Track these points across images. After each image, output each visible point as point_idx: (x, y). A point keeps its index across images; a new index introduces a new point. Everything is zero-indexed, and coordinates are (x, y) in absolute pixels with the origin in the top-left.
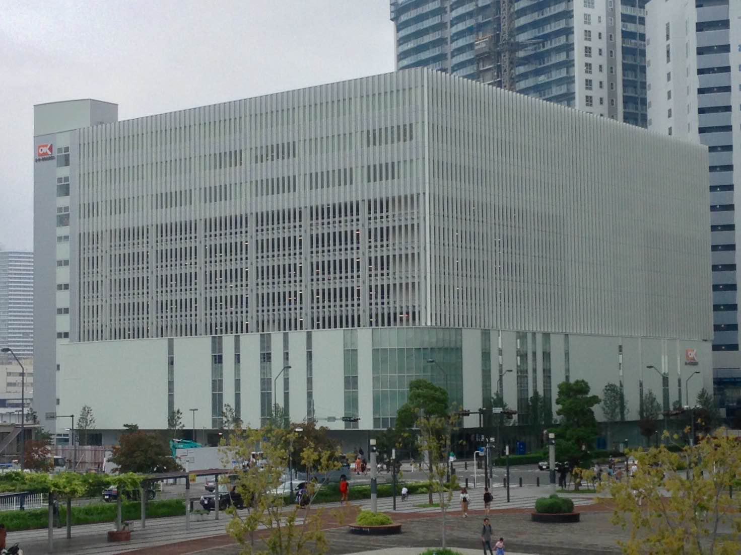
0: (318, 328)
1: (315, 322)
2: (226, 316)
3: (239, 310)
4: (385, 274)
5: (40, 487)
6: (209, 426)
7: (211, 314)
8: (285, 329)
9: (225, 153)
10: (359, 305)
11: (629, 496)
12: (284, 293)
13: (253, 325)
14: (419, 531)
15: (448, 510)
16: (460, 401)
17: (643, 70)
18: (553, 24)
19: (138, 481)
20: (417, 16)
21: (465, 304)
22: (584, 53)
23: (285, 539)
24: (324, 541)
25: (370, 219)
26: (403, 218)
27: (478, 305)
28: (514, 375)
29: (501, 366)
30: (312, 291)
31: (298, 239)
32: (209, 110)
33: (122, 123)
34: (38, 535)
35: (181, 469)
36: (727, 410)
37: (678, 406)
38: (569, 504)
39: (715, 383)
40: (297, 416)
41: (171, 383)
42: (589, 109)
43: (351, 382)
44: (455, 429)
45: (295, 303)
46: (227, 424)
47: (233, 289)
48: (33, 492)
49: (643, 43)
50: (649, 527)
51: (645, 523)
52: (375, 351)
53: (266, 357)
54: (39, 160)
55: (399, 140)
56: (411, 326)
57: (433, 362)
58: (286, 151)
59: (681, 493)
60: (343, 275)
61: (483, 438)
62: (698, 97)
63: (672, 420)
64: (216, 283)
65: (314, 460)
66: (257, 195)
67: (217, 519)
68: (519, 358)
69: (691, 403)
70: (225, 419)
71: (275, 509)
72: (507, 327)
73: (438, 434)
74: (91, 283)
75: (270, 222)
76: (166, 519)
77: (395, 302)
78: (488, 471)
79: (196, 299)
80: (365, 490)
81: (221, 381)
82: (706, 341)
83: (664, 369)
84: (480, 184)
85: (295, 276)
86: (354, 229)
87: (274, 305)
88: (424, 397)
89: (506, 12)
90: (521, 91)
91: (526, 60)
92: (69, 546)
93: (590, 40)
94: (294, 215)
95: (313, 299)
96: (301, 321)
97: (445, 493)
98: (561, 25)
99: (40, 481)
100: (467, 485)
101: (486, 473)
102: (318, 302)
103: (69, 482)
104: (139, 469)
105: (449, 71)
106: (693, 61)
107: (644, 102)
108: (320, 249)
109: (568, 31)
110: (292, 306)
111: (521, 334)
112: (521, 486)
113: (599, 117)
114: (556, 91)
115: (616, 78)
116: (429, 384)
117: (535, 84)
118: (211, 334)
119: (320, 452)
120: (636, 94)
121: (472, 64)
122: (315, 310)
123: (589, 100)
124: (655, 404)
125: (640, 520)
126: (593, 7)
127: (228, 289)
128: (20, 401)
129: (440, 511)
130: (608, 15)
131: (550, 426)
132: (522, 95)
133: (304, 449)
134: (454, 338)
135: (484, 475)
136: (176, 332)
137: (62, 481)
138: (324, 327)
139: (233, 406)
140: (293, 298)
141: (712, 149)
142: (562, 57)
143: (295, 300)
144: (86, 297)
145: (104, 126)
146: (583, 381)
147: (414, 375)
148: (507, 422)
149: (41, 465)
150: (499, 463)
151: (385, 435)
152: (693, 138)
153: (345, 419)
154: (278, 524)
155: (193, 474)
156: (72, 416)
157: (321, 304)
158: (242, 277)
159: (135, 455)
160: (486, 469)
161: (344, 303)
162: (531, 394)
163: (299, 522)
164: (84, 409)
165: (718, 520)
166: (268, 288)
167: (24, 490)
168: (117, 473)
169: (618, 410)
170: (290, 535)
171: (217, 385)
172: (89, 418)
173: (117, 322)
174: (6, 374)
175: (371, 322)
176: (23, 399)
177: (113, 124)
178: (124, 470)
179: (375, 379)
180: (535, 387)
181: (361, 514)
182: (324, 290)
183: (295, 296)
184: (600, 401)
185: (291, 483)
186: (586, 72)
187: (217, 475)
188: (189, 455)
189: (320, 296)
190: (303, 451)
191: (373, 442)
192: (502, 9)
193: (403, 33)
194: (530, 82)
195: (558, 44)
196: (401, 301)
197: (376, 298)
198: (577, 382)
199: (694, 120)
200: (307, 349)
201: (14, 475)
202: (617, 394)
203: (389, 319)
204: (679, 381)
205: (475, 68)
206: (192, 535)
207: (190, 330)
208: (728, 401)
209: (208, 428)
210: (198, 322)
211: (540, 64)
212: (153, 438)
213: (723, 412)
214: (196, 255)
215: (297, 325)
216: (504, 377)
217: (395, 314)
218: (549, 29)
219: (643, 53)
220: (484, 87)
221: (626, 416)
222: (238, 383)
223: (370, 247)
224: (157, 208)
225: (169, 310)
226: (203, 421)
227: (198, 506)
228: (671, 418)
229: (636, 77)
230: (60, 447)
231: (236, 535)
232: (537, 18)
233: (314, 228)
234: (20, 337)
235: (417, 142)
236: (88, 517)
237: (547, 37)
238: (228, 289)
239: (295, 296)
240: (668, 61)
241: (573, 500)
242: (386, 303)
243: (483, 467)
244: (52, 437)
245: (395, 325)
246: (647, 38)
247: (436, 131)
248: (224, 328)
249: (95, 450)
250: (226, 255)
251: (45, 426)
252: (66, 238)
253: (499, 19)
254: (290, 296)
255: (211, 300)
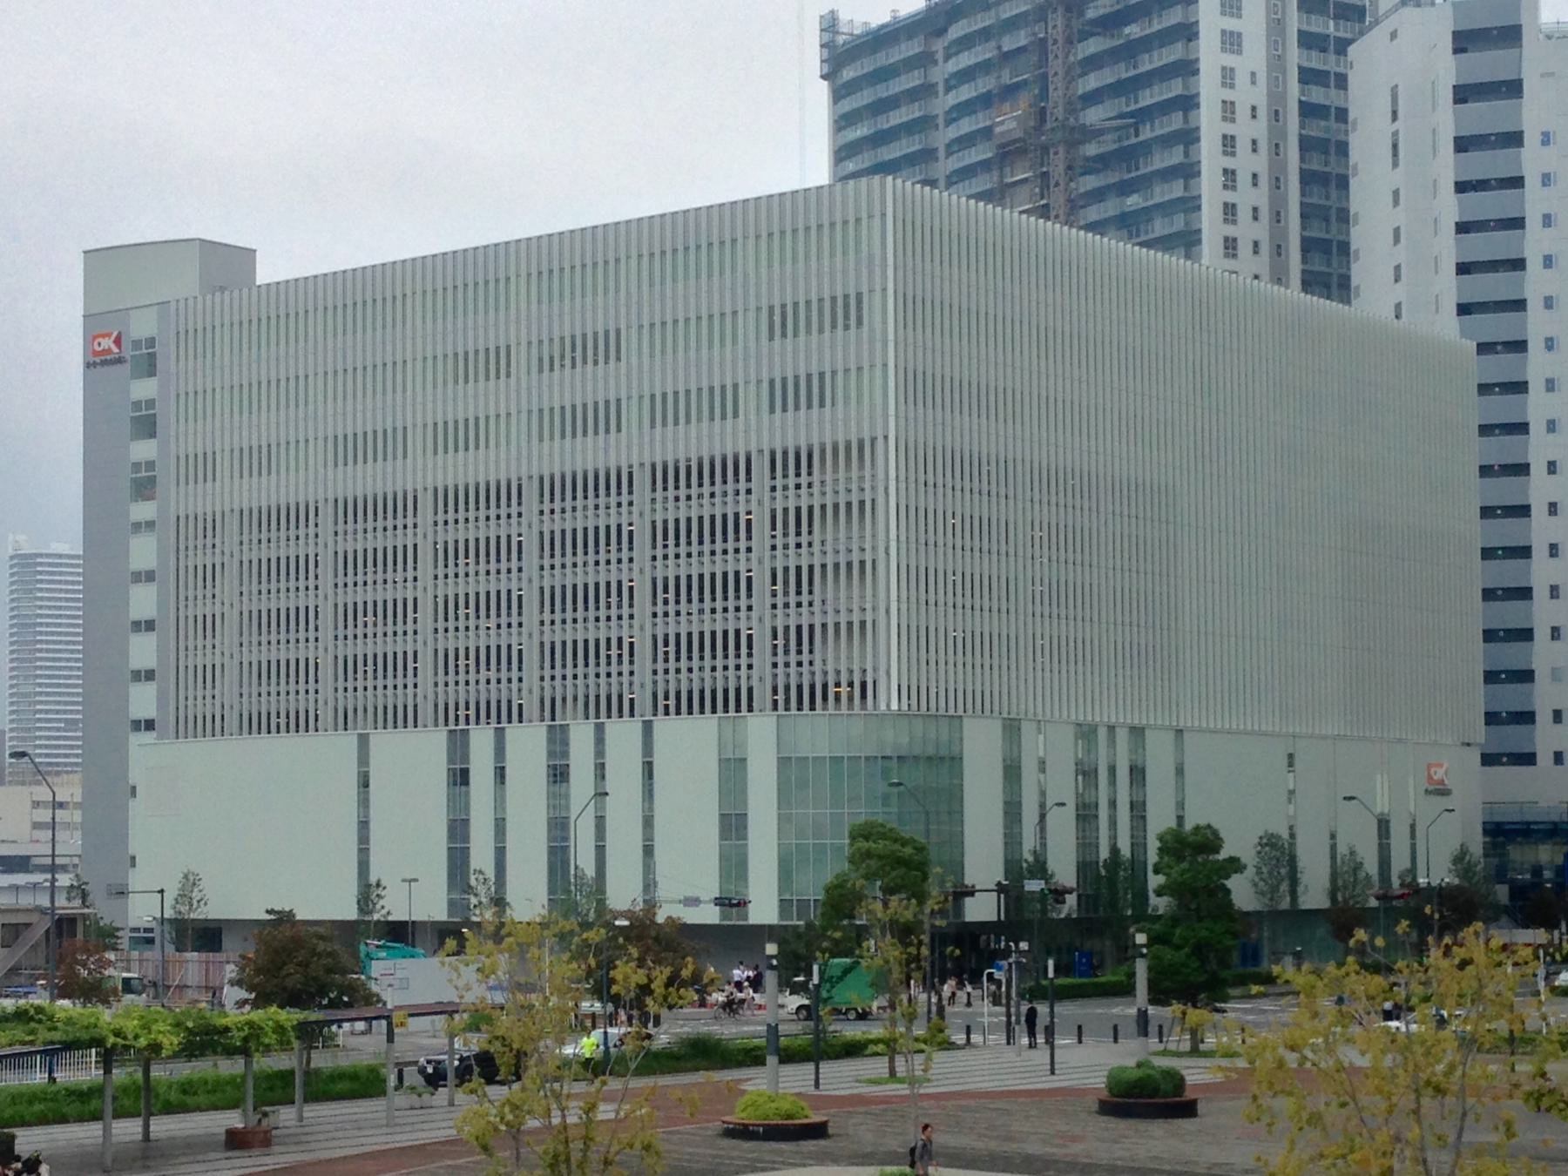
0: (667, 713)
1: (661, 703)
2: (482, 686)
3: (504, 675)
4: (805, 603)
5: (85, 1036)
6: (440, 914)
7: (446, 684)
8: (598, 717)
9: (477, 352)
10: (750, 667)
11: (1281, 1064)
12: (597, 642)
13: (531, 708)
14: (863, 1131)
15: (922, 1091)
16: (958, 868)
17: (1343, 183)
18: (1156, 88)
19: (288, 1025)
20: (875, 70)
21: (932, 663)
22: (1221, 148)
23: (576, 1146)
24: (657, 1153)
25: (773, 489)
26: (841, 488)
27: (969, 667)
28: (1070, 812)
29: (1043, 794)
30: (655, 638)
31: (743, 518)
32: (539, 247)
33: (263, 291)
34: (86, 1134)
35: (379, 1000)
36: (1511, 889)
37: (1408, 880)
38: (1177, 1081)
39: (1486, 832)
40: (623, 894)
41: (364, 825)
42: (1230, 264)
43: (733, 825)
44: (938, 923)
45: (620, 662)
46: (477, 912)
47: (492, 632)
48: (70, 1046)
49: (1343, 126)
50: (1324, 1129)
51: (1315, 1119)
52: (783, 762)
53: (559, 774)
54: (95, 364)
55: (834, 326)
56: (857, 710)
57: (899, 784)
58: (605, 347)
59: (1388, 1061)
60: (719, 605)
61: (1003, 944)
62: (1456, 239)
63: (1395, 908)
64: (457, 619)
65: (638, 986)
66: (541, 440)
67: (451, 1104)
68: (1080, 778)
69: (1437, 872)
70: (474, 901)
71: (556, 1086)
72: (1065, 713)
73: (904, 932)
74: (255, 614)
75: (472, 505)
76: (345, 1103)
77: (824, 662)
78: (1013, 1010)
79: (415, 653)
80: (757, 1048)
81: (466, 822)
82: (1468, 745)
83: (1381, 805)
84: (993, 418)
85: (620, 607)
86: (742, 510)
87: (575, 666)
88: (880, 857)
89: (1060, 61)
90: (1092, 227)
91: (1101, 163)
92: (145, 1158)
93: (1233, 120)
94: (616, 482)
95: (655, 655)
96: (520, 705)
97: (916, 1056)
98: (1176, 88)
99: (86, 1023)
100: (968, 1039)
101: (1009, 1015)
102: (666, 660)
103: (146, 1027)
104: (293, 999)
105: (942, 183)
106: (1446, 166)
107: (1344, 248)
108: (671, 551)
109: (1188, 103)
110: (614, 669)
111: (1086, 729)
112: (1080, 1041)
113: (1248, 281)
114: (1160, 228)
115: (1286, 201)
116: (891, 830)
117: (1118, 212)
118: (447, 725)
119: (650, 969)
120: (1327, 232)
121: (989, 170)
122: (660, 677)
123: (1230, 245)
124: (1362, 875)
125: (1305, 1116)
126: (1240, 52)
127: (482, 632)
128: (48, 861)
129: (908, 1092)
130: (1270, 68)
131: (1142, 916)
132: (1090, 235)
133: (618, 963)
134: (945, 737)
135: (1004, 1019)
136: (376, 722)
137: (131, 1025)
138: (678, 713)
139: (490, 873)
140: (614, 652)
141: (1484, 348)
142: (1176, 156)
143: (620, 656)
144: (191, 647)
145: (227, 293)
146: (1209, 826)
147: (862, 813)
148: (1054, 909)
149: (94, 992)
150: (1036, 993)
151: (799, 936)
152: (1448, 325)
153: (719, 902)
154: (564, 1116)
155: (402, 1013)
156: (162, 891)
157: (672, 665)
158: (509, 607)
159: (284, 972)
160: (1008, 1006)
161: (719, 663)
162: (1104, 854)
163: (605, 1112)
164: (186, 877)
165: (1464, 1115)
166: (467, 637)
167: (52, 1043)
168: (248, 1007)
169: (1284, 887)
170: (587, 1140)
171: (459, 830)
172: (196, 895)
173: (254, 700)
174: (29, 804)
175: (775, 703)
176: (53, 856)
177: (245, 291)
178: (256, 1004)
179: (783, 819)
180: (1113, 838)
181: (747, 1097)
182: (678, 636)
183: (620, 647)
184: (1245, 867)
185: (606, 1033)
186: (1225, 187)
187: (451, 1013)
188: (399, 974)
189: (672, 648)
190: (615, 967)
191: (771, 949)
192: (1051, 57)
193: (848, 105)
194: (1110, 208)
195: (1166, 130)
196: (837, 658)
197: (787, 652)
198: (1197, 828)
199: (1449, 288)
200: (644, 756)
201: (32, 1012)
202: (1283, 853)
203: (808, 697)
204: (1413, 827)
205: (995, 179)
206: (398, 1138)
207: (403, 717)
208: (1514, 870)
209: (437, 918)
210: (420, 700)
211: (1129, 171)
212: (321, 938)
213: (1502, 893)
214: (415, 562)
215: (621, 707)
216: (1048, 817)
217: (825, 686)
218: (1147, 98)
219: (1343, 149)
220: (1012, 219)
221: (1301, 900)
222: (500, 826)
223: (774, 548)
224: (435, 452)
225: (360, 675)
226: (431, 905)
227: (412, 1077)
228: (1394, 903)
229: (1329, 265)
230: (135, 954)
231: (477, 1138)
232: (1124, 75)
233: (658, 506)
234: (58, 729)
235: (872, 330)
236: (184, 1100)
237: (1144, 115)
238: (482, 632)
239: (620, 647)
240: (1395, 164)
241: (1184, 1072)
242: (806, 664)
243: (1004, 1001)
244: (119, 934)
245: (825, 708)
246: (1351, 116)
247: (910, 305)
248: (472, 712)
249: (207, 963)
250: (478, 563)
251: (103, 910)
252: (150, 525)
253: (1045, 76)
254: (609, 648)
255: (446, 656)
